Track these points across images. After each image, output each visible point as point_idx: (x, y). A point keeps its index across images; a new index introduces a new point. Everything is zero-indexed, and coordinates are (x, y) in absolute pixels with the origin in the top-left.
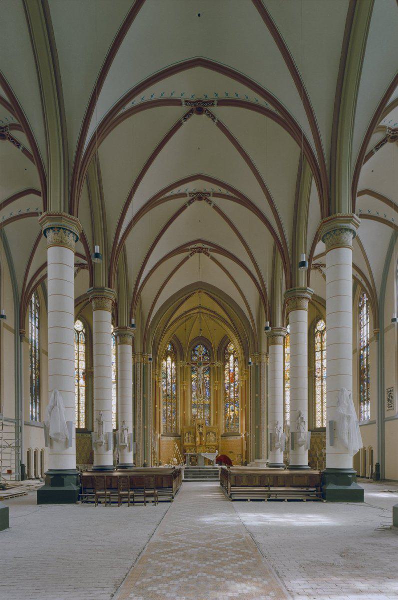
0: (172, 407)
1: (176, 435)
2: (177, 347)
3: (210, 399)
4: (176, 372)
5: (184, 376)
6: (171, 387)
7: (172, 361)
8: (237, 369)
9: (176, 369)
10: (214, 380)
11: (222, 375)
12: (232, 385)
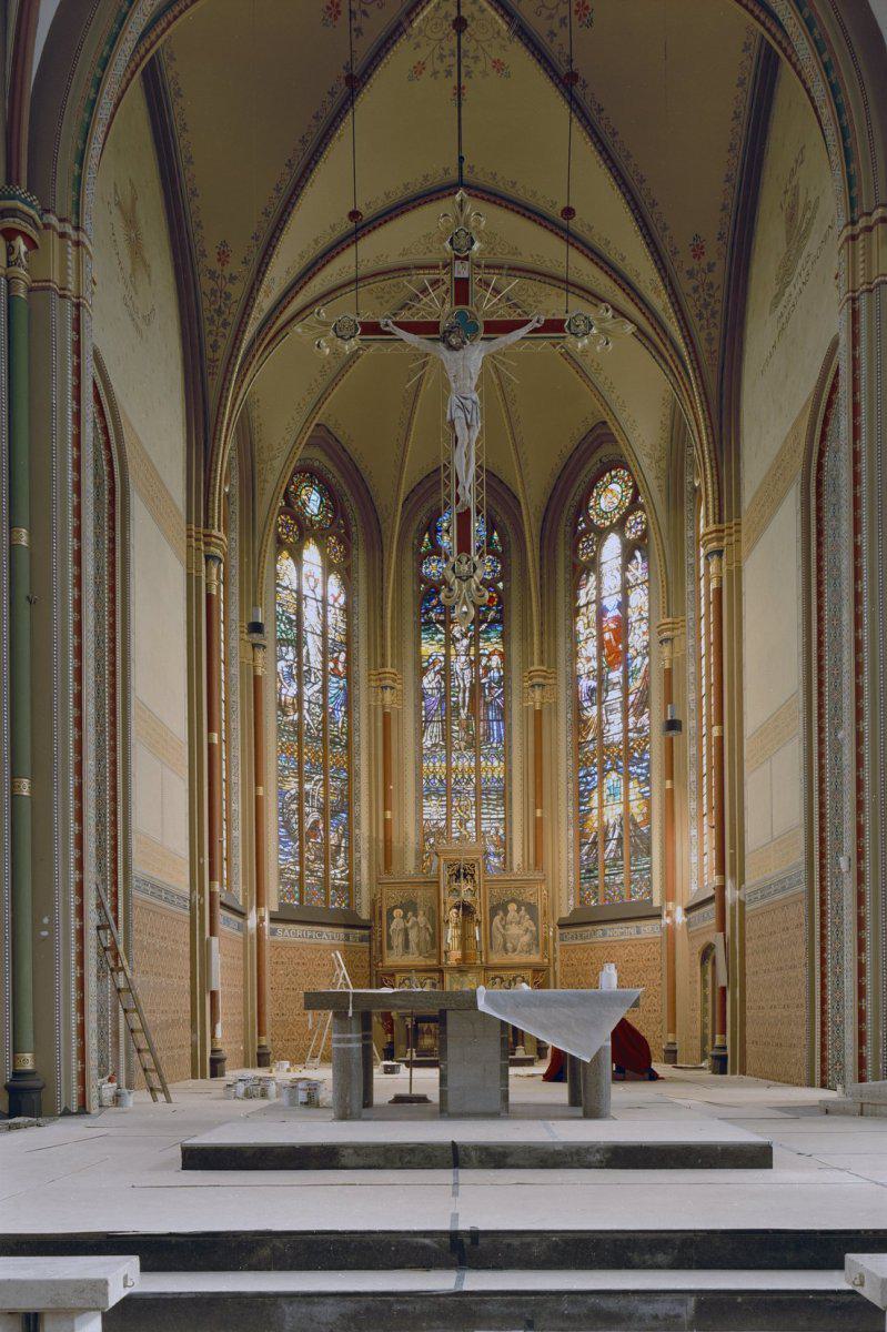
0: (325, 785)
1: (349, 921)
2: (351, 505)
3: (506, 755)
4: (348, 624)
5: (383, 647)
6: (324, 690)
7: (329, 568)
8: (638, 598)
9: (348, 610)
10: (526, 661)
11: (561, 640)
12: (615, 676)
